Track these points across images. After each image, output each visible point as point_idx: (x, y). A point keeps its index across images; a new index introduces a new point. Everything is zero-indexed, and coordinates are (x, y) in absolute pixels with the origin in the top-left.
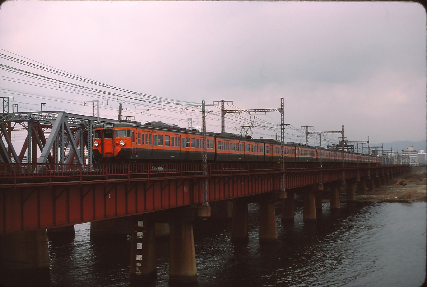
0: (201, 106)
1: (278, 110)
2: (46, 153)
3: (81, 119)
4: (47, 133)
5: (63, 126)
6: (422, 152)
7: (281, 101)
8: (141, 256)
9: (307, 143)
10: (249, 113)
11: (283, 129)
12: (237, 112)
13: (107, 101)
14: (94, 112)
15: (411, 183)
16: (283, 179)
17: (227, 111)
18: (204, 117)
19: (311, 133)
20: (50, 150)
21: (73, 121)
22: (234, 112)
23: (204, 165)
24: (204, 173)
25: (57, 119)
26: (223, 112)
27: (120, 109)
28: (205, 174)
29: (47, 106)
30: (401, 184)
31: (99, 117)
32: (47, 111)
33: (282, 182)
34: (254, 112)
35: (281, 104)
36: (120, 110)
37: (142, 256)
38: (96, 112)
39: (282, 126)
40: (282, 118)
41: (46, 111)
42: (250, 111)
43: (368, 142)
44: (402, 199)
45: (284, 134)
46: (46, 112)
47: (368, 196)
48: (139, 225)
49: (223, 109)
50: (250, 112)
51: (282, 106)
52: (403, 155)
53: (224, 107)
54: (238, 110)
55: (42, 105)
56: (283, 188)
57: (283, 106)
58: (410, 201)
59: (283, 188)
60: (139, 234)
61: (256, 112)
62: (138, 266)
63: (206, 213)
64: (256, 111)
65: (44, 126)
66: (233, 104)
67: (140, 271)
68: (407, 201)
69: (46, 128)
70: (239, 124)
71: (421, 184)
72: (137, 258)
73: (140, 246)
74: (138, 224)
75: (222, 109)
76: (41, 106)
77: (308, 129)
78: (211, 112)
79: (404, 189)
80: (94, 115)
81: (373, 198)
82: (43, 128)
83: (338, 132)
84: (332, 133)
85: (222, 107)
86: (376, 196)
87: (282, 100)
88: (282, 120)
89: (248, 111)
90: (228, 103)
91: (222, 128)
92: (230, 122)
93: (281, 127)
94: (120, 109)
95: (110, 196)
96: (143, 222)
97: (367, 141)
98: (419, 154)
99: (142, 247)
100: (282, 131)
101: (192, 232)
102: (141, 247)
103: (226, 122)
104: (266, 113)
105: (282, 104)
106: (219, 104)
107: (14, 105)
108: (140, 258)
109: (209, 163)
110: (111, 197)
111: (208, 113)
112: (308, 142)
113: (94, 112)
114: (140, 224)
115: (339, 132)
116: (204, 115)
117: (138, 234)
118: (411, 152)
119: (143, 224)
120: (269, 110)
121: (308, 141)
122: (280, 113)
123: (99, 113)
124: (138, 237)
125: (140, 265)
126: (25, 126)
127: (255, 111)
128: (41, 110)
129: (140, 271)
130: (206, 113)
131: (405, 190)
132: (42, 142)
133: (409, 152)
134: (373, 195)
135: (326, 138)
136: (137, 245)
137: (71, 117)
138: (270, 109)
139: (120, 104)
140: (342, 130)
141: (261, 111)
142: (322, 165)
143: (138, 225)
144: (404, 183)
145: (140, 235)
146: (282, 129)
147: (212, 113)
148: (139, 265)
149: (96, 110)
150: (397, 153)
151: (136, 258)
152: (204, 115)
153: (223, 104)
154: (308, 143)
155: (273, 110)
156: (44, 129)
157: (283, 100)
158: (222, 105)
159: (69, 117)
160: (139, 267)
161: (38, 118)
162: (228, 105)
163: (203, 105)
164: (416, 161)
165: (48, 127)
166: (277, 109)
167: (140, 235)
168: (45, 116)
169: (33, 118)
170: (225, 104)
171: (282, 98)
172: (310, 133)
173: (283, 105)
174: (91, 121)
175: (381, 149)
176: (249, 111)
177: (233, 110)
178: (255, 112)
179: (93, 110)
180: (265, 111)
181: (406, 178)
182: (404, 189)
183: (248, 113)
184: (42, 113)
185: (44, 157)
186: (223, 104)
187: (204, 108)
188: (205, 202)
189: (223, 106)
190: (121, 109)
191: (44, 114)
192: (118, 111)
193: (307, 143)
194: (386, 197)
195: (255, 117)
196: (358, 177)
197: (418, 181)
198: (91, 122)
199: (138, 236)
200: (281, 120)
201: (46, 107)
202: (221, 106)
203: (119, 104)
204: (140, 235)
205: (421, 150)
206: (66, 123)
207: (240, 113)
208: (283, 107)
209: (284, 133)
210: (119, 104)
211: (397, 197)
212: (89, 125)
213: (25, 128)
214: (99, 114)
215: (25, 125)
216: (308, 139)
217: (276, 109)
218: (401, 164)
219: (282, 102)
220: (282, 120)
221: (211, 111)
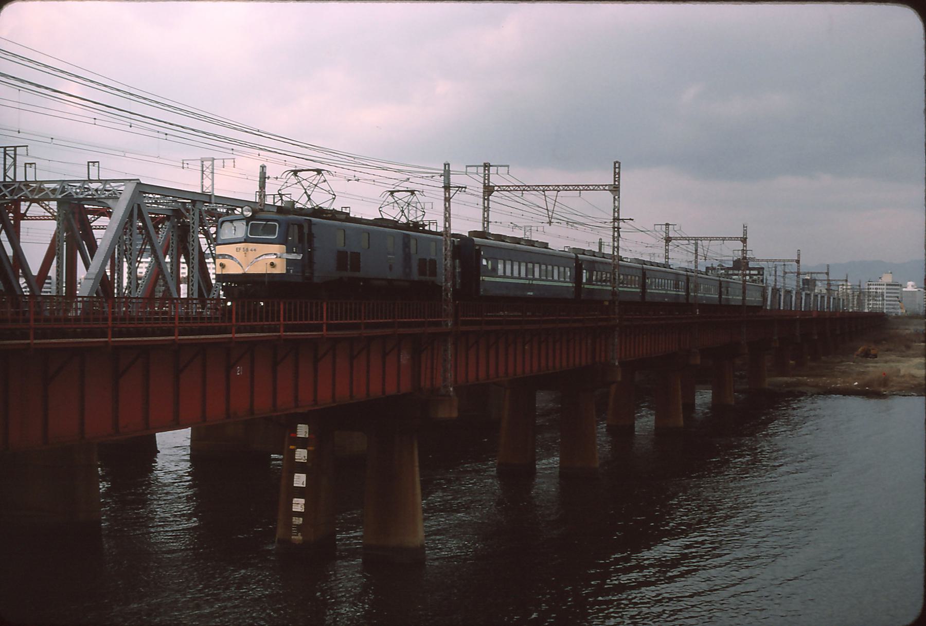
0: (441, 176)
1: (607, 187)
2: (98, 271)
3: (175, 199)
4: (99, 226)
5: (135, 211)
6: (912, 286)
7: (615, 168)
9: (667, 260)
10: (543, 193)
11: (617, 229)
13: (233, 160)
14: (204, 184)
15: (886, 353)
17: (496, 188)
18: (447, 200)
19: (676, 239)
20: (912, 281)
21: (156, 203)
22: (511, 190)
23: (445, 307)
25: (122, 198)
26: (487, 190)
27: (263, 178)
28: (447, 325)
29: (100, 169)
30: (867, 355)
31: (215, 195)
32: (101, 178)
34: (554, 190)
35: (615, 175)
36: (262, 180)
37: (305, 501)
38: (207, 183)
39: (616, 223)
40: (615, 206)
43: (798, 262)
44: (867, 388)
45: (618, 240)
46: (99, 181)
47: (794, 379)
48: (301, 434)
49: (486, 181)
50: (547, 190)
51: (617, 179)
52: (873, 292)
53: (489, 179)
54: (519, 186)
55: (88, 165)
57: (619, 180)
58: (885, 393)
60: (300, 454)
61: (559, 191)
62: (297, 523)
63: (448, 412)
64: (558, 189)
65: (93, 212)
66: (508, 173)
69: (96, 217)
70: (476, 206)
71: (908, 356)
72: (293, 507)
73: (300, 480)
75: (484, 183)
76: (87, 166)
77: (668, 230)
78: (464, 189)
79: (872, 366)
80: (204, 190)
81: (806, 384)
82: (89, 216)
83: (733, 239)
84: (722, 241)
85: (484, 177)
86: (812, 380)
87: (617, 165)
88: (616, 210)
89: (542, 189)
90: (497, 170)
91: (484, 224)
92: (500, 212)
93: (614, 224)
94: (263, 178)
95: (239, 371)
96: (309, 426)
97: (797, 259)
98: (904, 289)
99: (305, 483)
100: (616, 234)
101: (416, 452)
102: (303, 482)
103: (455, 201)
104: (580, 193)
106: (479, 172)
107: (27, 165)
108: (300, 505)
110: (241, 373)
111: (457, 190)
112: (488, 222)
113: (203, 182)
114: (303, 431)
115: (736, 239)
116: (447, 196)
117: (296, 453)
118: (887, 285)
119: (308, 431)
121: (668, 256)
122: (612, 193)
123: (215, 185)
124: (296, 460)
125: (301, 522)
126: (51, 211)
127: (557, 188)
128: (87, 175)
130: (452, 192)
131: (876, 368)
132: (87, 247)
133: (884, 285)
134: (805, 378)
135: (707, 252)
136: (295, 477)
137: (152, 194)
139: (263, 167)
140: (744, 235)
143: (298, 433)
144: (873, 352)
145: (302, 456)
146: (616, 229)
147: (465, 191)
148: (298, 521)
149: (207, 178)
150: (858, 287)
151: (292, 506)
152: (447, 196)
153: (487, 172)
154: (668, 262)
155: (597, 187)
156: (93, 217)
157: (619, 165)
158: (485, 175)
159: (149, 193)
160: (299, 527)
161: (80, 193)
163: (447, 174)
166: (606, 185)
167: (301, 455)
168: (97, 190)
169: (70, 193)
170: (491, 172)
171: (617, 162)
172: (673, 238)
173: (619, 177)
174: (198, 202)
175: (825, 277)
176: (544, 188)
177: (509, 186)
178: (556, 192)
179: (203, 179)
180: (578, 189)
182: (872, 366)
183: (541, 192)
184: (90, 184)
186: (487, 172)
187: (449, 179)
189: (487, 177)
190: (266, 178)
191: (94, 186)
192: (258, 183)
193: (666, 262)
195: (555, 201)
198: (197, 204)
200: (614, 210)
201: (99, 170)
202: (482, 175)
203: (261, 166)
204: (301, 455)
205: (910, 281)
206: (141, 206)
207: (524, 192)
208: (619, 182)
209: (620, 239)
210: (259, 167)
211: (856, 383)
213: (51, 215)
214: (215, 187)
215: (52, 209)
216: (668, 253)
217: (602, 185)
218: (866, 311)
219: (617, 170)
220: (616, 210)
221: (462, 187)
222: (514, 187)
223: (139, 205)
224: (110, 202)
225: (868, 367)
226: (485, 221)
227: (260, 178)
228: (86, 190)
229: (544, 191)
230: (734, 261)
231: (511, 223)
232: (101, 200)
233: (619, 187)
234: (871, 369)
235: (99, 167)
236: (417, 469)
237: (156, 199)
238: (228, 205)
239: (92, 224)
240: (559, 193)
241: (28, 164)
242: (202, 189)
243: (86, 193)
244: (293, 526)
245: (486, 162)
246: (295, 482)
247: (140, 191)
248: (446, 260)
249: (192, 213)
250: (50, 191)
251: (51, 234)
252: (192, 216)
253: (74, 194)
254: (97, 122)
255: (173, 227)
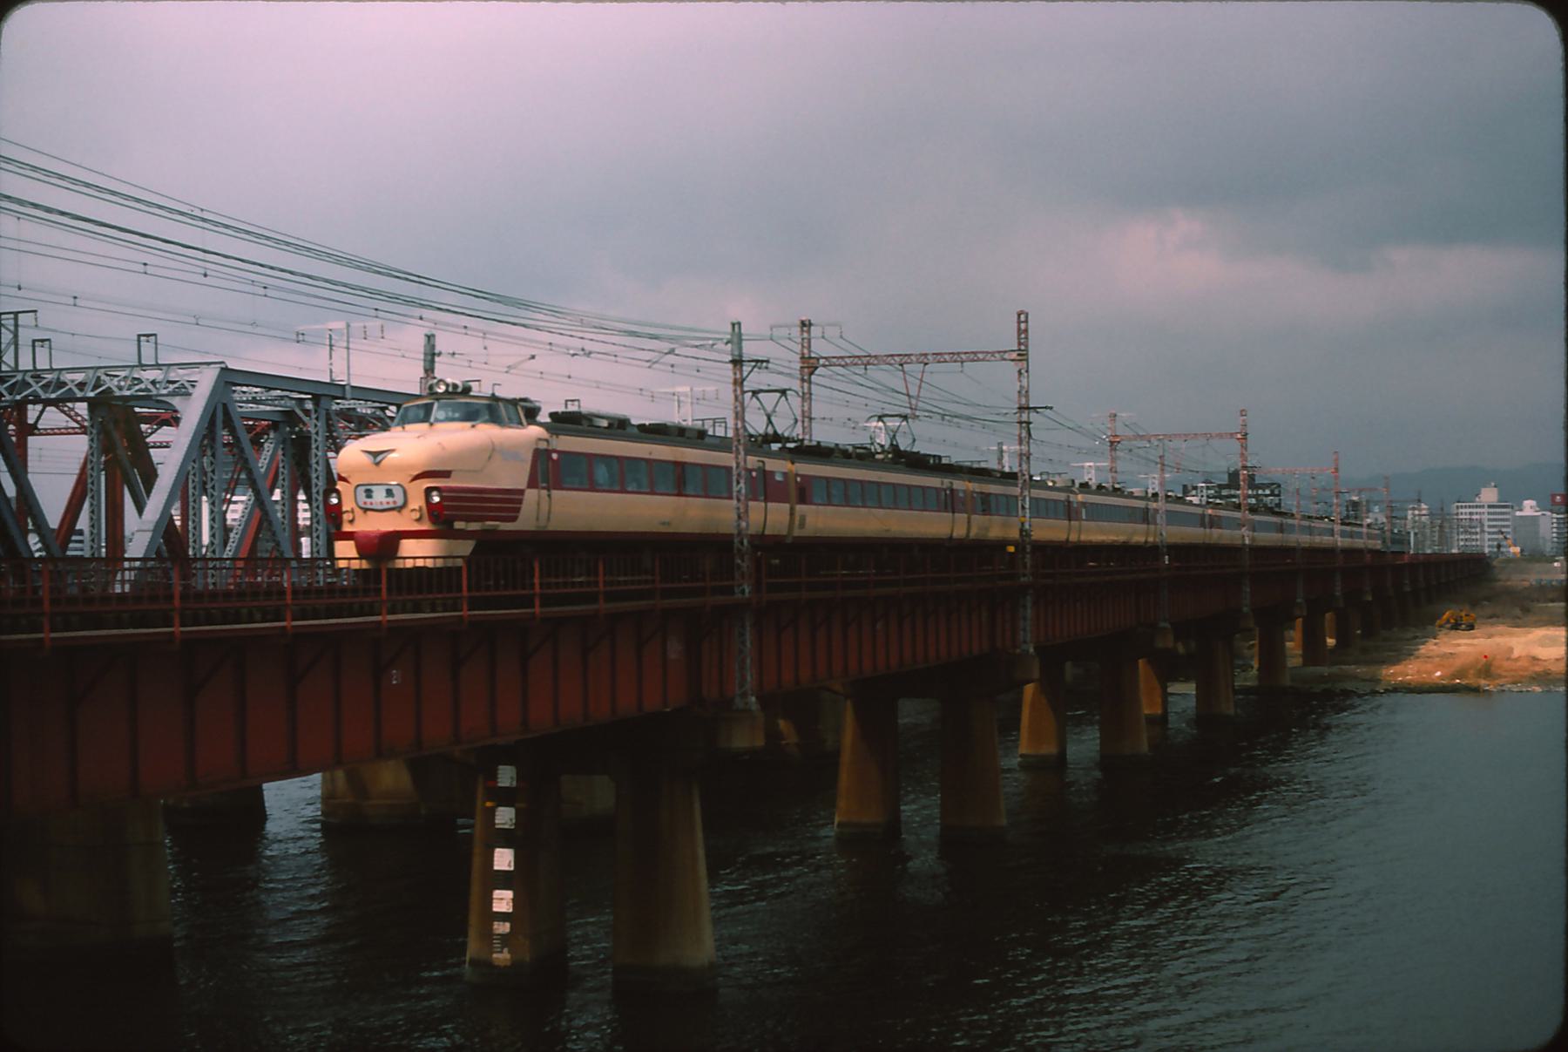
0: (727, 343)
2: (158, 516)
5: (219, 416)
6: (1531, 507)
7: (1019, 322)
8: (509, 894)
10: (900, 368)
12: (856, 364)
16: (1025, 607)
20: (1533, 499)
22: (847, 364)
24: (741, 588)
27: (431, 356)
28: (743, 592)
29: (159, 347)
32: (160, 362)
33: (1025, 619)
35: (1019, 335)
36: (429, 358)
40: (1021, 386)
41: (157, 362)
42: (902, 360)
44: (1458, 681)
45: (1028, 443)
47: (1335, 669)
49: (806, 351)
50: (906, 363)
51: (1022, 341)
52: (1466, 519)
55: (139, 341)
56: (1025, 642)
58: (1487, 688)
59: (1025, 642)
61: (926, 364)
65: (148, 419)
67: (506, 950)
68: (1479, 687)
69: (155, 427)
72: (494, 905)
73: (504, 859)
74: (497, 778)
75: (803, 354)
76: (136, 342)
78: (764, 364)
81: (1355, 677)
82: (144, 427)
86: (1364, 670)
88: (1023, 392)
93: (1021, 416)
94: (431, 356)
96: (517, 768)
98: (1518, 513)
99: (512, 864)
100: (1024, 434)
101: (697, 806)
102: (510, 862)
105: (1022, 332)
107: (37, 343)
108: (505, 902)
109: (759, 553)
111: (754, 367)
112: (811, 419)
114: (506, 776)
117: (497, 813)
118: (1490, 507)
119: (515, 776)
120: (974, 356)
124: (497, 827)
126: (79, 418)
127: (923, 358)
129: (506, 950)
133: (1483, 507)
134: (1353, 667)
136: (496, 854)
137: (247, 386)
138: (946, 354)
139: (430, 338)
141: (945, 361)
142: (1167, 557)
143: (499, 780)
145: (507, 819)
146: (1024, 425)
148: (503, 928)
153: (805, 335)
156: (149, 428)
157: (1027, 317)
158: (803, 339)
160: (505, 939)
162: (826, 336)
164: (1508, 533)
165: (163, 420)
166: (1005, 352)
167: (505, 817)
170: (812, 335)
173: (1026, 338)
177: (842, 358)
178: (922, 365)
181: (1474, 603)
185: (149, 535)
187: (740, 348)
188: (744, 695)
194: (1402, 674)
196: (1299, 600)
197: (1518, 612)
199: (497, 821)
200: (1019, 392)
201: (156, 348)
202: (800, 340)
203: (426, 335)
204: (505, 817)
205: (1527, 499)
207: (868, 367)
208: (1027, 346)
210: (423, 337)
211: (1438, 674)
212: (313, 412)
215: (80, 415)
217: (999, 352)
220: (1024, 392)
221: (762, 361)
222: (852, 359)
223: (225, 405)
224: (176, 402)
225: (1459, 645)
227: (425, 354)
228: (136, 382)
229: (901, 365)
230: (1230, 474)
231: (849, 419)
232: (159, 398)
233: (1027, 354)
234: (1462, 649)
235: (156, 343)
236: (699, 835)
237: (254, 395)
238: (374, 402)
239: (148, 440)
240: (927, 366)
241: (144, 335)
242: (331, 376)
243: (137, 388)
244: (495, 937)
245: (804, 318)
246: (495, 863)
247: (226, 382)
248: (738, 483)
249: (314, 416)
250: (76, 385)
251: (79, 458)
252: (315, 421)
253: (115, 389)
254: (150, 270)
255: (284, 442)
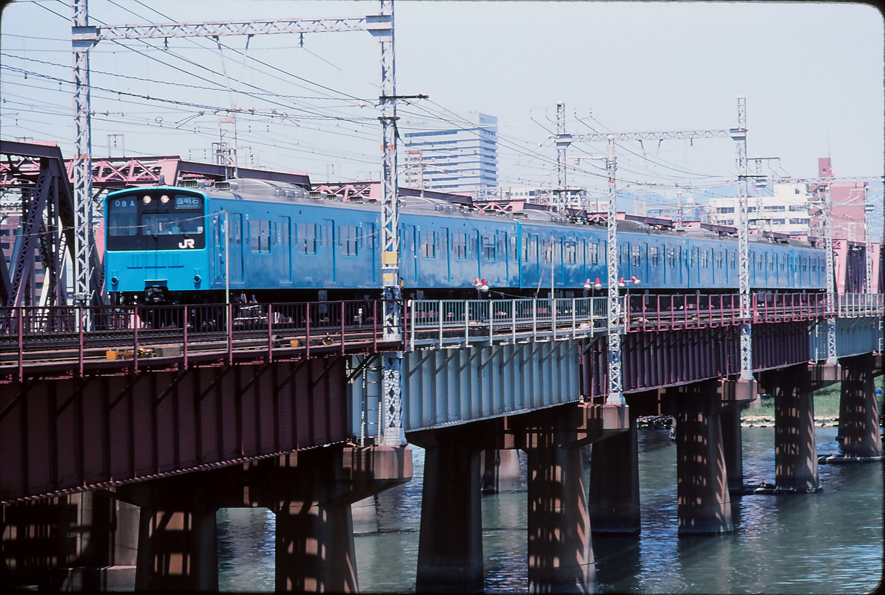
61: (251, 35)
220: (118, 135)
226: (79, 108)
